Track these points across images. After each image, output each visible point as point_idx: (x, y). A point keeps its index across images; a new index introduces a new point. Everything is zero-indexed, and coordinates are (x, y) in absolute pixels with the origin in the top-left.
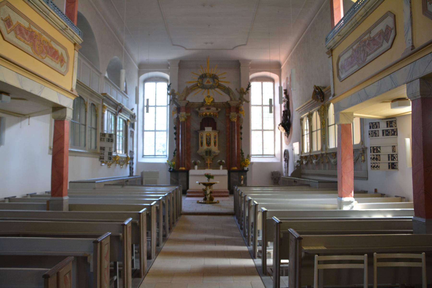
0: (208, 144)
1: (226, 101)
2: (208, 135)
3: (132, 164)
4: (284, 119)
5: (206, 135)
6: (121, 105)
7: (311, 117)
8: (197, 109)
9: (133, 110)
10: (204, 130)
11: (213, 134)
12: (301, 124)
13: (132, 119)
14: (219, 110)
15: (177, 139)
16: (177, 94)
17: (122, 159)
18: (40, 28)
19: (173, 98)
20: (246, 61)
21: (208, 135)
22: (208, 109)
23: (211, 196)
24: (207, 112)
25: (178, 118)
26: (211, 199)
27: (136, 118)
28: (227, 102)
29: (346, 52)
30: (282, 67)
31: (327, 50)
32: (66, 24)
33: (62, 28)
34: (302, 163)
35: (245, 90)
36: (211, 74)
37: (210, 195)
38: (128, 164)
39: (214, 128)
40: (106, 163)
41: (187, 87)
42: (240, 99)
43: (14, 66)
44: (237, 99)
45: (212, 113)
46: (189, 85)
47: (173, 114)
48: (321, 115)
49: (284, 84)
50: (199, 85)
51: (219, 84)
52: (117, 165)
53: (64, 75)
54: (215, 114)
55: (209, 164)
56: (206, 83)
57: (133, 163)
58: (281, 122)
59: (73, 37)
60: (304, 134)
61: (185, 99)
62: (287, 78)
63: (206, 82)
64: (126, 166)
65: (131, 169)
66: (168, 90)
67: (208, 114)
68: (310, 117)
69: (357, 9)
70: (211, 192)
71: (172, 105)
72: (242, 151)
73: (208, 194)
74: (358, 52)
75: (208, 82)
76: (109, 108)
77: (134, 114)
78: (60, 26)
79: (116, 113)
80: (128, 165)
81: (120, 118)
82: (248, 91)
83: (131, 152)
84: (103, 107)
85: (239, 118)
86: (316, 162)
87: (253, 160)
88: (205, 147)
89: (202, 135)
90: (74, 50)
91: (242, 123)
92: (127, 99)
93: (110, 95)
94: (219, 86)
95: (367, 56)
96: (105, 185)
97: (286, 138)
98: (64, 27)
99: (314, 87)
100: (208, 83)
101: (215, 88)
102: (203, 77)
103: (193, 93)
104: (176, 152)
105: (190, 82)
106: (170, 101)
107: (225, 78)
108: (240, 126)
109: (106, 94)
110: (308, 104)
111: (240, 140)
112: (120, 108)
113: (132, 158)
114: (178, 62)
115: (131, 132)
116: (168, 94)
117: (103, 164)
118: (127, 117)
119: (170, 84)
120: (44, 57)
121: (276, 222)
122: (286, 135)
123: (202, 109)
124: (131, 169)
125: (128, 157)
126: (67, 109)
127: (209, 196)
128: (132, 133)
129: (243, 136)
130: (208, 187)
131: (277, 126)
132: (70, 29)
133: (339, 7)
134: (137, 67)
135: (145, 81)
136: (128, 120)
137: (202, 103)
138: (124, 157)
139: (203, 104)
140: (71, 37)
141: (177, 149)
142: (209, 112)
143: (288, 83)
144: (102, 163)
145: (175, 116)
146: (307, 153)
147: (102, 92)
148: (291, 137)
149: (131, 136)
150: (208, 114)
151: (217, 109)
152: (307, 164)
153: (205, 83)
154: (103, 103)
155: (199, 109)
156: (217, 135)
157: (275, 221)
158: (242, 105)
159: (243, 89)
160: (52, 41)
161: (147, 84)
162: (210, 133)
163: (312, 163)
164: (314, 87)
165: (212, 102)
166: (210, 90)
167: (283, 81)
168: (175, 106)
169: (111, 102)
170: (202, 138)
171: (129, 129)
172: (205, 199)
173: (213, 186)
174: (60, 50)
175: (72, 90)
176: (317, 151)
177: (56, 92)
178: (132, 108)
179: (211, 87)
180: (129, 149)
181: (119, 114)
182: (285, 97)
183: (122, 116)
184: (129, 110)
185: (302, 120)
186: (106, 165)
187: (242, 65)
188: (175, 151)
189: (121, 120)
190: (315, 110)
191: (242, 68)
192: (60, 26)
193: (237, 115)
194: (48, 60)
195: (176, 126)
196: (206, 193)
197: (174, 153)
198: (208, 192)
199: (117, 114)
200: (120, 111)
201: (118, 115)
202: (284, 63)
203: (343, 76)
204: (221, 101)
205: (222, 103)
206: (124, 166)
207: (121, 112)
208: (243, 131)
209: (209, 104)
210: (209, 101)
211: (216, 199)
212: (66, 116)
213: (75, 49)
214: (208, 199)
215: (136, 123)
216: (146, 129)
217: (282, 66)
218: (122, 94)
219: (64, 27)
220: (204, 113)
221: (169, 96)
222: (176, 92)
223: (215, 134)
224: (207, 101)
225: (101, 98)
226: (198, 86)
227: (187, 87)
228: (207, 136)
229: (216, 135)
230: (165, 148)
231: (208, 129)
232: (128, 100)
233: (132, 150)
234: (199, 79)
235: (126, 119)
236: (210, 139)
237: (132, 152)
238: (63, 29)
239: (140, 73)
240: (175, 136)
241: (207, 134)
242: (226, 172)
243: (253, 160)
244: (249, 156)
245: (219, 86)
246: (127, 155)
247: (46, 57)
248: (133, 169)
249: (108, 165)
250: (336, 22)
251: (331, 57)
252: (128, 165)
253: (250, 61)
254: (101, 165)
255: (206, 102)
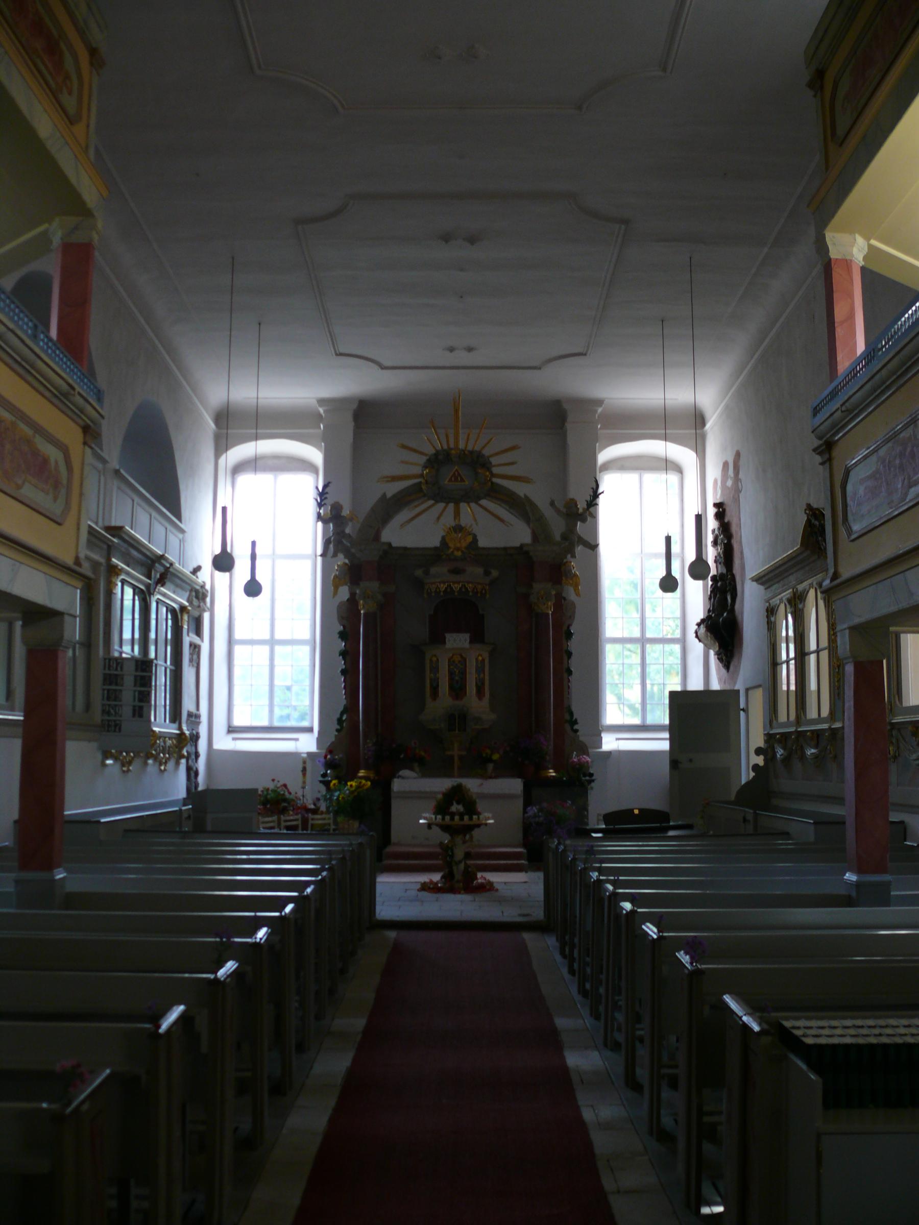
0: (458, 690)
1: (518, 545)
2: (457, 659)
3: (193, 757)
4: (713, 606)
5: (449, 660)
6: (166, 559)
7: (800, 606)
8: (419, 573)
9: (199, 574)
10: (444, 642)
11: (476, 656)
12: (772, 628)
13: (195, 602)
14: (495, 573)
15: (349, 673)
16: (351, 519)
17: (165, 742)
18: (14, 406)
19: (336, 533)
20: (589, 405)
21: (457, 659)
22: (456, 571)
23: (467, 867)
24: (454, 583)
25: (353, 600)
26: (469, 876)
27: (208, 600)
28: (522, 546)
29: (871, 455)
30: (708, 426)
31: (817, 443)
32: (71, 381)
33: (59, 392)
34: (774, 754)
35: (581, 506)
36: (466, 452)
37: (465, 863)
38: (183, 756)
39: (477, 637)
40: (116, 759)
41: (384, 495)
42: (565, 537)
43: (17, 549)
44: (558, 537)
45: (470, 586)
46: (393, 489)
47: (336, 587)
48: (829, 602)
49: (716, 481)
50: (424, 487)
51: (492, 483)
52: (150, 761)
53: (59, 524)
54: (479, 587)
55: (456, 758)
56: (450, 480)
57: (197, 755)
58: (706, 614)
59: (82, 411)
60: (778, 661)
61: (377, 537)
62: (726, 465)
63: (448, 480)
64: (178, 764)
65: (192, 773)
66: (320, 505)
67: (456, 587)
68: (796, 604)
69: (882, 352)
70: (468, 855)
71: (335, 555)
72: (571, 714)
73: (460, 862)
74: (889, 469)
75: (456, 477)
76: (128, 574)
77: (203, 587)
78: (56, 388)
79: (148, 586)
80: (183, 761)
81: (123, 582)
82: (592, 509)
83: (190, 715)
84: (113, 571)
85: (561, 603)
86: (816, 757)
87: (609, 743)
88: (445, 701)
89: (434, 659)
90: (82, 446)
91: (572, 617)
92: (181, 536)
93: (132, 529)
94: (497, 493)
95: (910, 487)
96: (126, 831)
97: (724, 671)
98: (65, 387)
99: (806, 510)
100: (456, 480)
101: (479, 498)
102: (438, 461)
103: (404, 515)
104: (344, 718)
105: (394, 479)
106: (327, 543)
107: (513, 463)
108: (565, 628)
109: (121, 528)
110: (790, 564)
111: (565, 675)
112: (162, 569)
113: (195, 738)
114: (355, 406)
115: (193, 646)
116: (319, 517)
117: (109, 762)
118: (180, 599)
119: (325, 487)
120: (20, 482)
121: (650, 938)
122: (720, 660)
123: (434, 570)
124: (193, 775)
125: (182, 733)
126: (67, 618)
127: (462, 866)
128: (195, 648)
129: (574, 664)
130: (459, 839)
131: (692, 627)
132: (79, 394)
133: (851, 316)
134: (213, 425)
135: (238, 469)
136: (183, 609)
137: (436, 548)
138: (171, 736)
139: (435, 556)
140: (77, 411)
141: (350, 708)
142: (459, 583)
143: (729, 483)
144: (107, 758)
145: (344, 593)
146: (787, 724)
147: (107, 524)
148: (738, 667)
149: (191, 661)
150: (456, 587)
151: (487, 573)
152: (787, 760)
153: (446, 482)
154: (109, 560)
155: (427, 573)
156: (487, 662)
157: (648, 934)
158: (574, 556)
159: (576, 505)
160: (37, 436)
161: (245, 479)
162: (464, 655)
163: (803, 757)
164: (807, 512)
165: (471, 543)
166: (463, 506)
167: (714, 472)
168: (341, 559)
169: (135, 553)
170: (435, 669)
171: (188, 638)
172: (449, 877)
173: (476, 833)
174: (53, 454)
175: (77, 562)
176: (820, 720)
177: (42, 575)
178: (195, 566)
179: (470, 497)
180: (188, 705)
181: (157, 590)
182: (719, 529)
183: (164, 595)
184: (187, 571)
185: (771, 612)
186: (118, 765)
187: (570, 418)
188: (342, 714)
189: (129, 592)
190: (811, 586)
191: (568, 426)
192: (56, 388)
193: (554, 593)
194: (29, 491)
195: (344, 627)
196: (452, 856)
197: (340, 721)
198: (459, 853)
199: (152, 591)
200: (161, 581)
201: (155, 593)
202: (712, 417)
203: (857, 527)
204: (501, 544)
205: (505, 549)
206: (171, 765)
207: (162, 586)
208: (574, 645)
209: (459, 554)
210: (458, 545)
211: (483, 877)
212: (62, 637)
213: (85, 443)
214: (458, 876)
215: (206, 616)
216: (238, 635)
217: (709, 421)
218: (147, 507)
219: (65, 387)
220: (443, 587)
221: (320, 524)
222: (346, 512)
223: (480, 658)
224: (451, 545)
225: (105, 543)
226: (421, 490)
227: (384, 495)
228: (451, 662)
229: (483, 660)
230: (307, 702)
231: (457, 641)
232: (182, 541)
233: (192, 709)
234: (425, 467)
235: (176, 606)
236: (463, 673)
237: (194, 718)
238: (61, 394)
239: (222, 444)
240: (341, 664)
241: (452, 657)
242: (515, 785)
243: (609, 743)
244: (597, 729)
245: (497, 493)
246: (180, 728)
247: (23, 483)
248: (197, 773)
249: (123, 765)
250: (844, 364)
251: (827, 465)
252: (183, 761)
253: (600, 402)
254: (104, 765)
255: (448, 548)
